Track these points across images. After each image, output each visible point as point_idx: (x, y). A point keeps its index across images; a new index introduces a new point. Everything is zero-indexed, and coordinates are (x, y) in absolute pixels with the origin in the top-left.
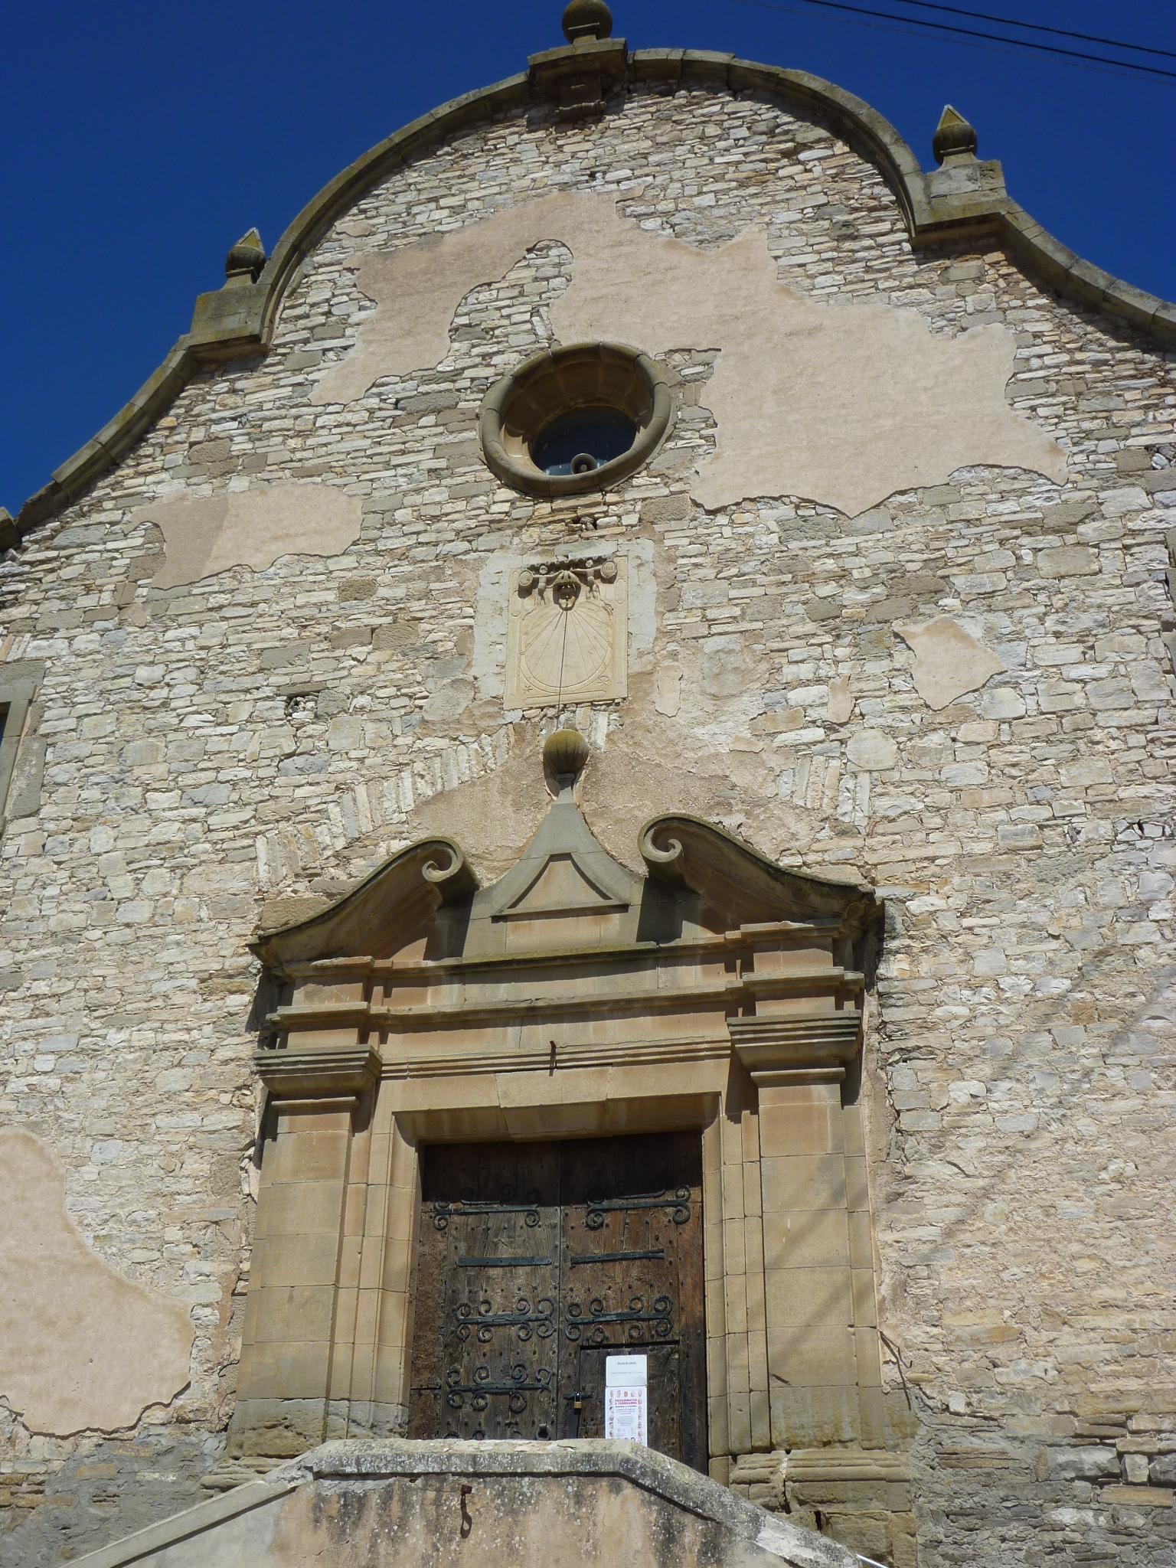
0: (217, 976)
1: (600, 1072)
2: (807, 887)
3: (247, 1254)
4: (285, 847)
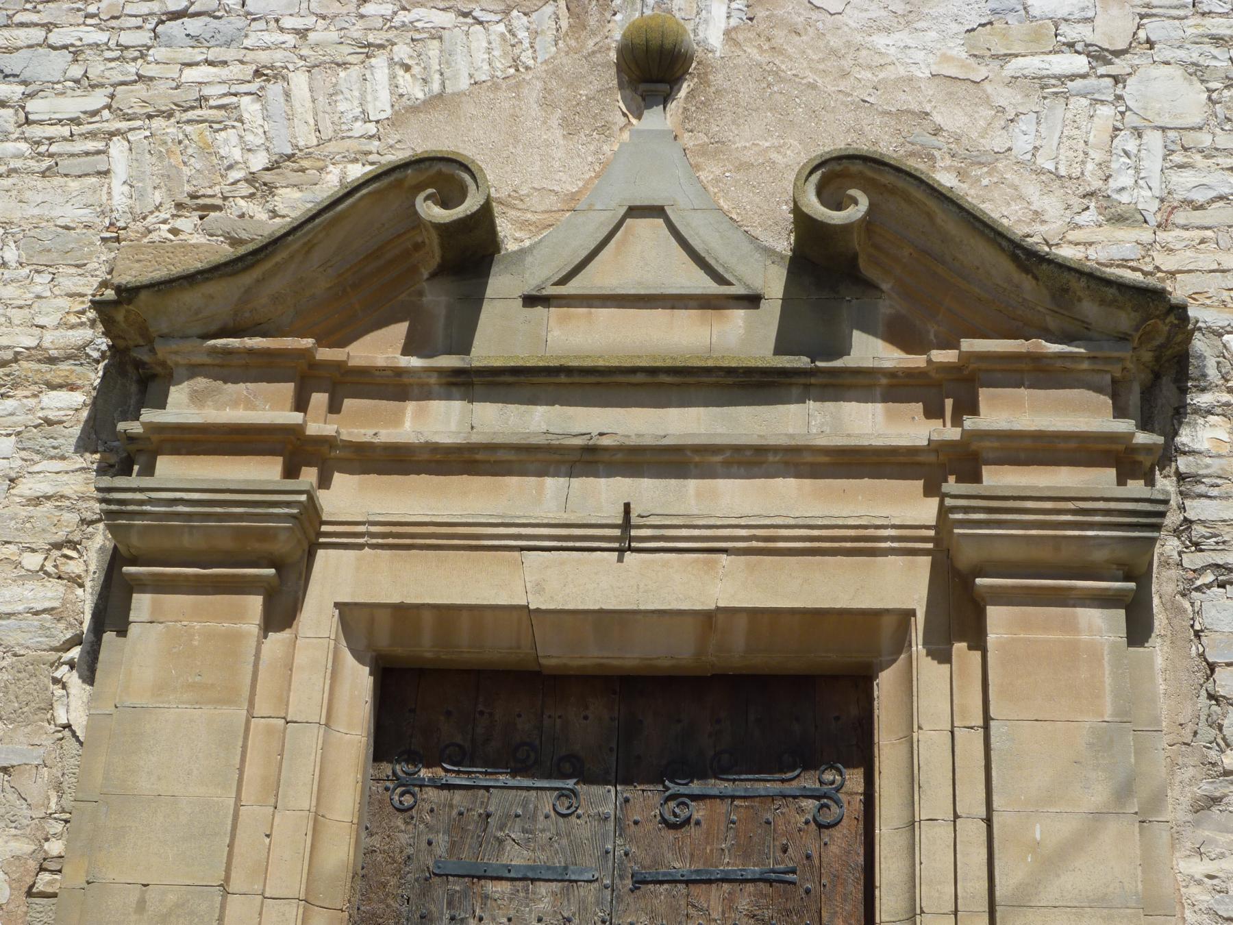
0: (28, 358)
1: (706, 563)
2: (1078, 285)
3: (59, 827)
4: (161, 157)
